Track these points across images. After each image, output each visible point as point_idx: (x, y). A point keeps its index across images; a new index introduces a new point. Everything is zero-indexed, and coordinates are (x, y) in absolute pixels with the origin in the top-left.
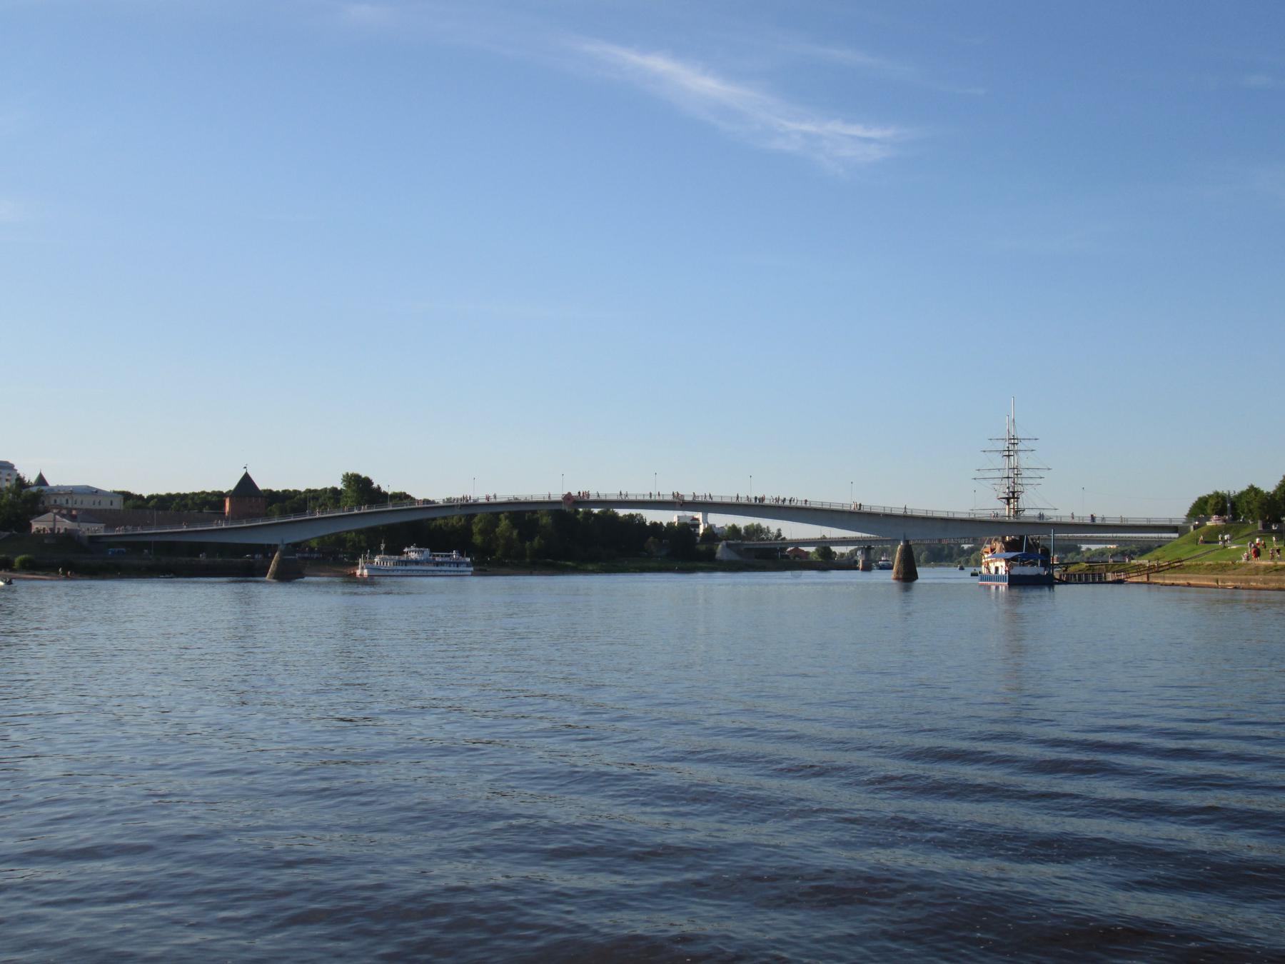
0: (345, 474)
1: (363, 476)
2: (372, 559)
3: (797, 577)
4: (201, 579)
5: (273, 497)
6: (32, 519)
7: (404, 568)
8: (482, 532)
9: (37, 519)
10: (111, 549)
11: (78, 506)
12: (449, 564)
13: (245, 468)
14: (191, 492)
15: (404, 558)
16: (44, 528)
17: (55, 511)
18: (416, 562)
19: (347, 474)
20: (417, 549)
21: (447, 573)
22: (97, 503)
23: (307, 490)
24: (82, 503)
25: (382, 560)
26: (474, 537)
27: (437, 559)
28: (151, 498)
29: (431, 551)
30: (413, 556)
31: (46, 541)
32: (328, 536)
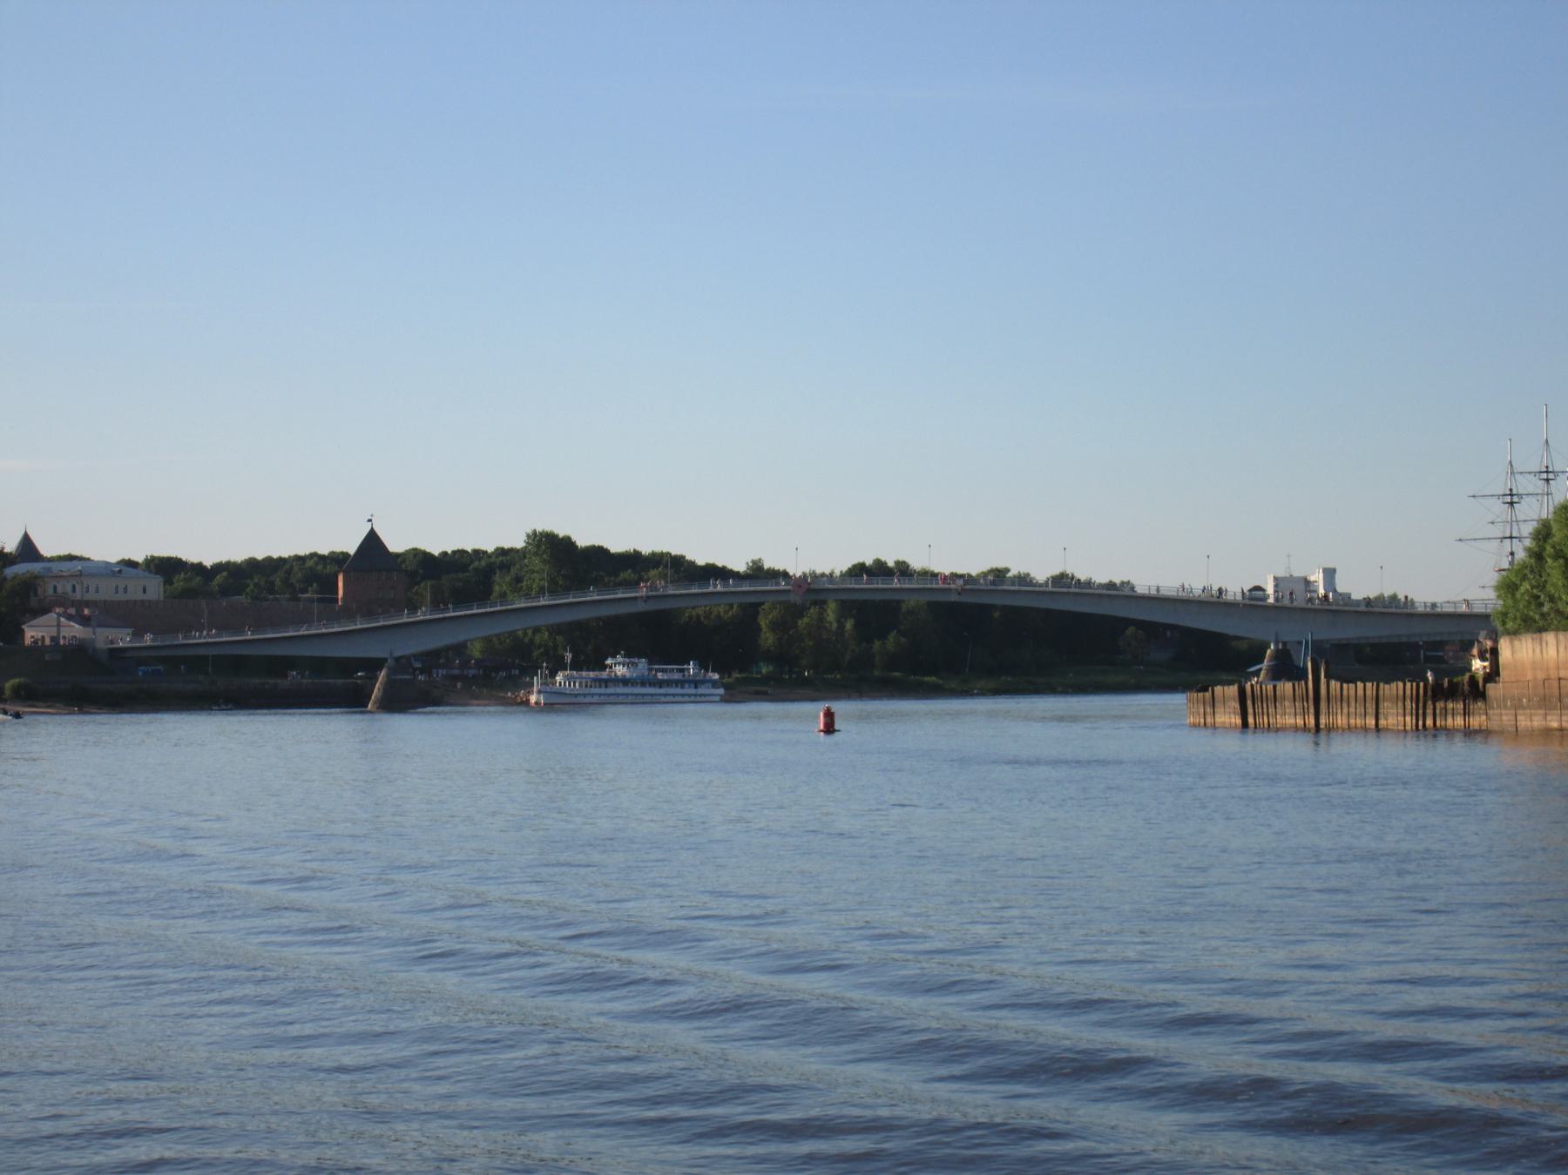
0: (530, 531)
1: (561, 535)
2: (553, 674)
3: (1018, 703)
4: (309, 711)
5: (425, 565)
6: (24, 623)
7: (603, 690)
8: (775, 626)
9: (32, 623)
10: (142, 668)
11: (91, 596)
12: (678, 683)
13: (370, 520)
14: (292, 554)
15: (604, 675)
16: (43, 637)
17: (57, 610)
18: (625, 681)
19: (535, 530)
20: (627, 660)
21: (677, 699)
22: (121, 590)
23: (497, 549)
24: (97, 591)
25: (567, 678)
26: (763, 636)
27: (660, 676)
28: (219, 568)
29: (650, 663)
30: (620, 671)
31: (47, 657)
32: (498, 636)
